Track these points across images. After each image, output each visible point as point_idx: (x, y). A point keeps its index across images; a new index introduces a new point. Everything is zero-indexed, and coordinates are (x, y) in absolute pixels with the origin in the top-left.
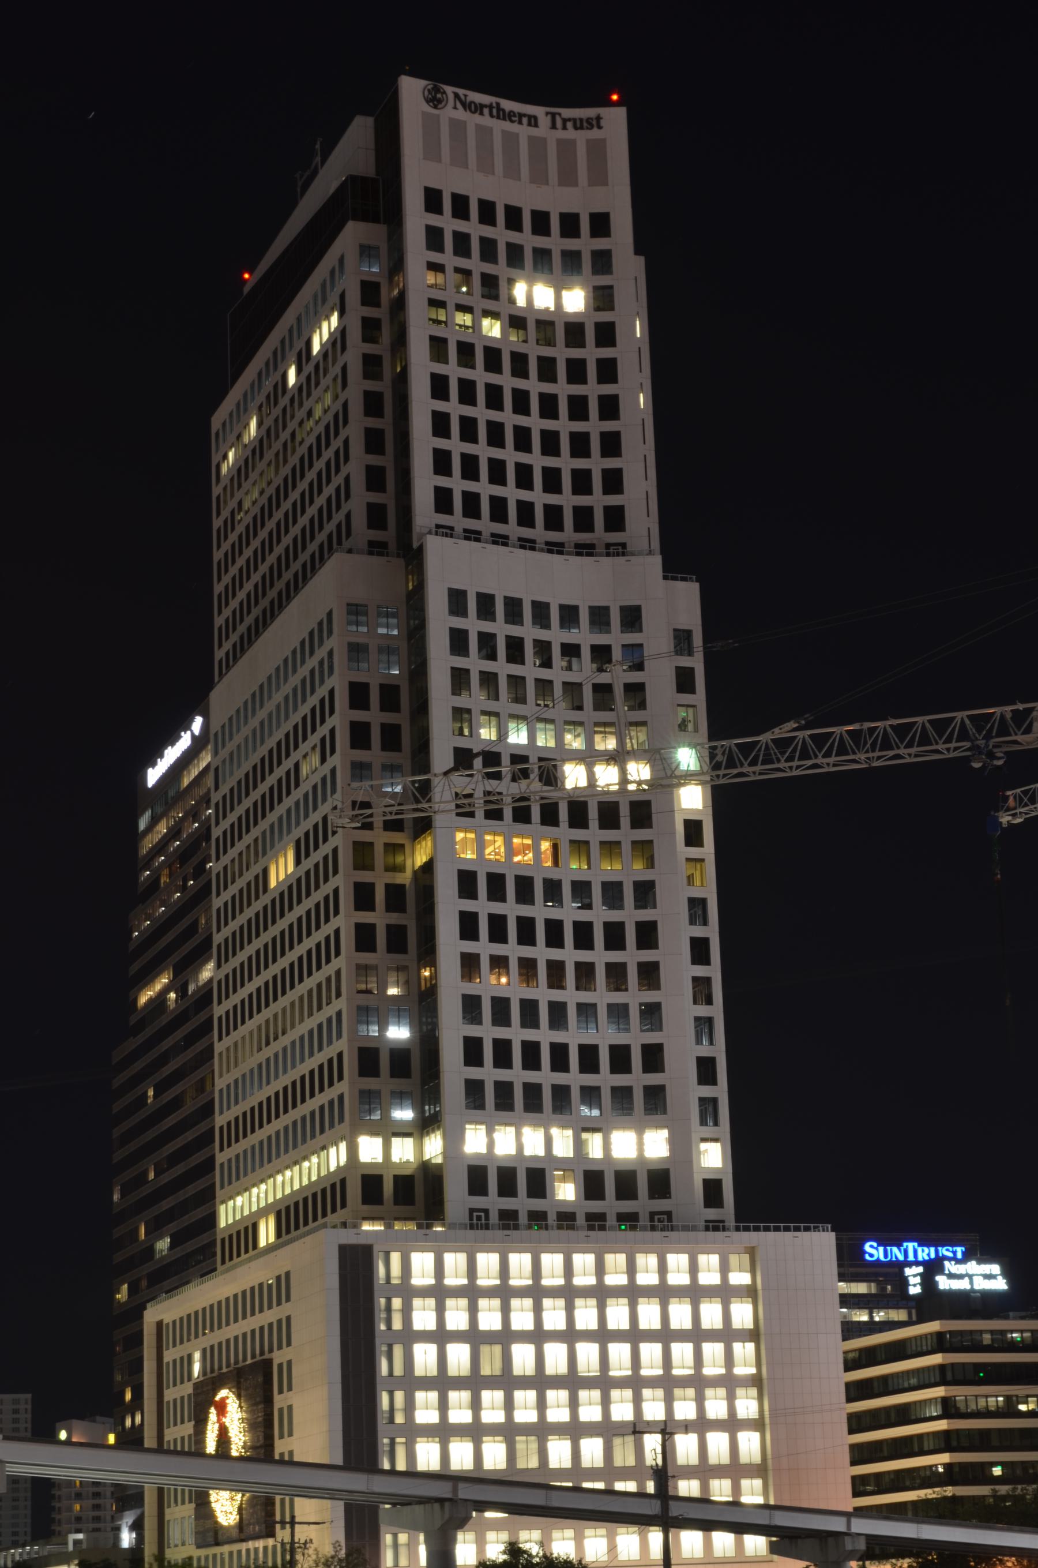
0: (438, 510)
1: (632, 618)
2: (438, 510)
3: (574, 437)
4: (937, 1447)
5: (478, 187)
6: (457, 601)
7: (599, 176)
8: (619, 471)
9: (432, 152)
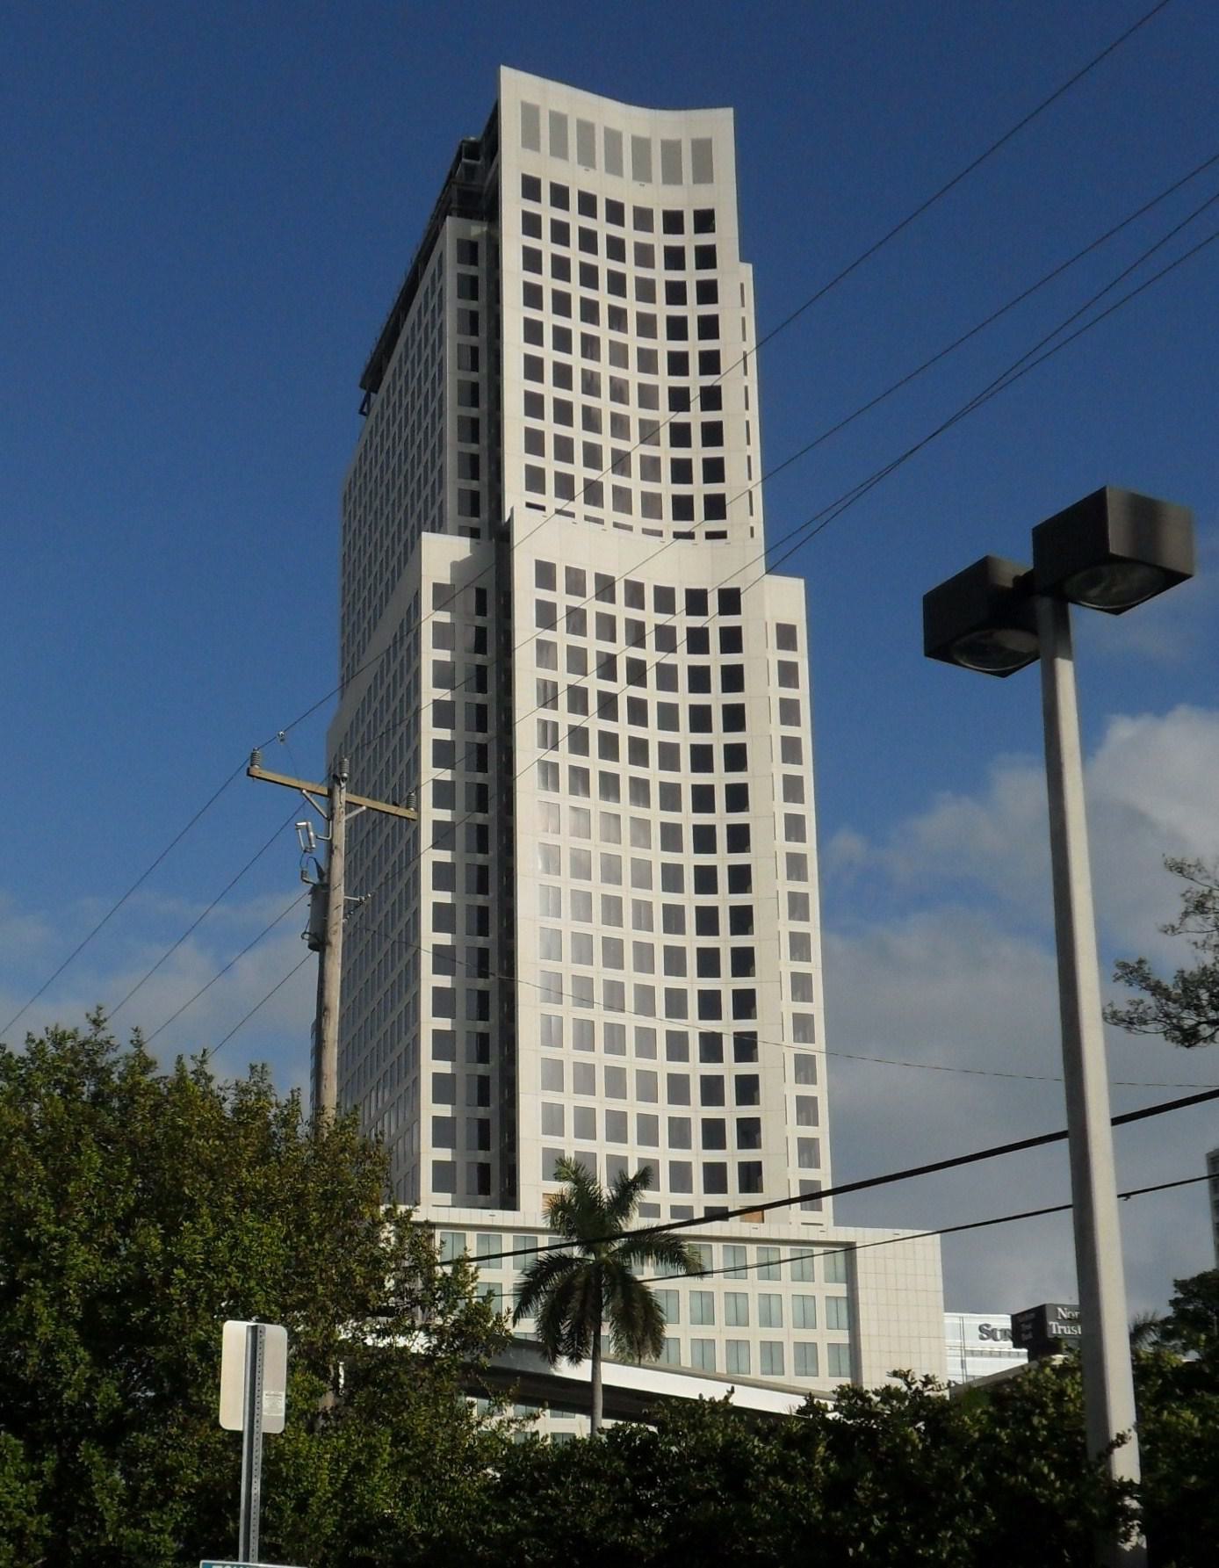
0: (528, 413)
1: (730, 601)
2: (528, 413)
3: (697, 790)
4: (1040, 757)
5: (578, 179)
6: (545, 575)
7: (704, 173)
8: (752, 992)
9: (530, 140)
